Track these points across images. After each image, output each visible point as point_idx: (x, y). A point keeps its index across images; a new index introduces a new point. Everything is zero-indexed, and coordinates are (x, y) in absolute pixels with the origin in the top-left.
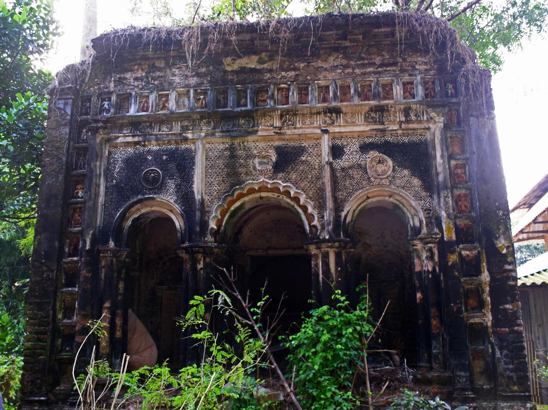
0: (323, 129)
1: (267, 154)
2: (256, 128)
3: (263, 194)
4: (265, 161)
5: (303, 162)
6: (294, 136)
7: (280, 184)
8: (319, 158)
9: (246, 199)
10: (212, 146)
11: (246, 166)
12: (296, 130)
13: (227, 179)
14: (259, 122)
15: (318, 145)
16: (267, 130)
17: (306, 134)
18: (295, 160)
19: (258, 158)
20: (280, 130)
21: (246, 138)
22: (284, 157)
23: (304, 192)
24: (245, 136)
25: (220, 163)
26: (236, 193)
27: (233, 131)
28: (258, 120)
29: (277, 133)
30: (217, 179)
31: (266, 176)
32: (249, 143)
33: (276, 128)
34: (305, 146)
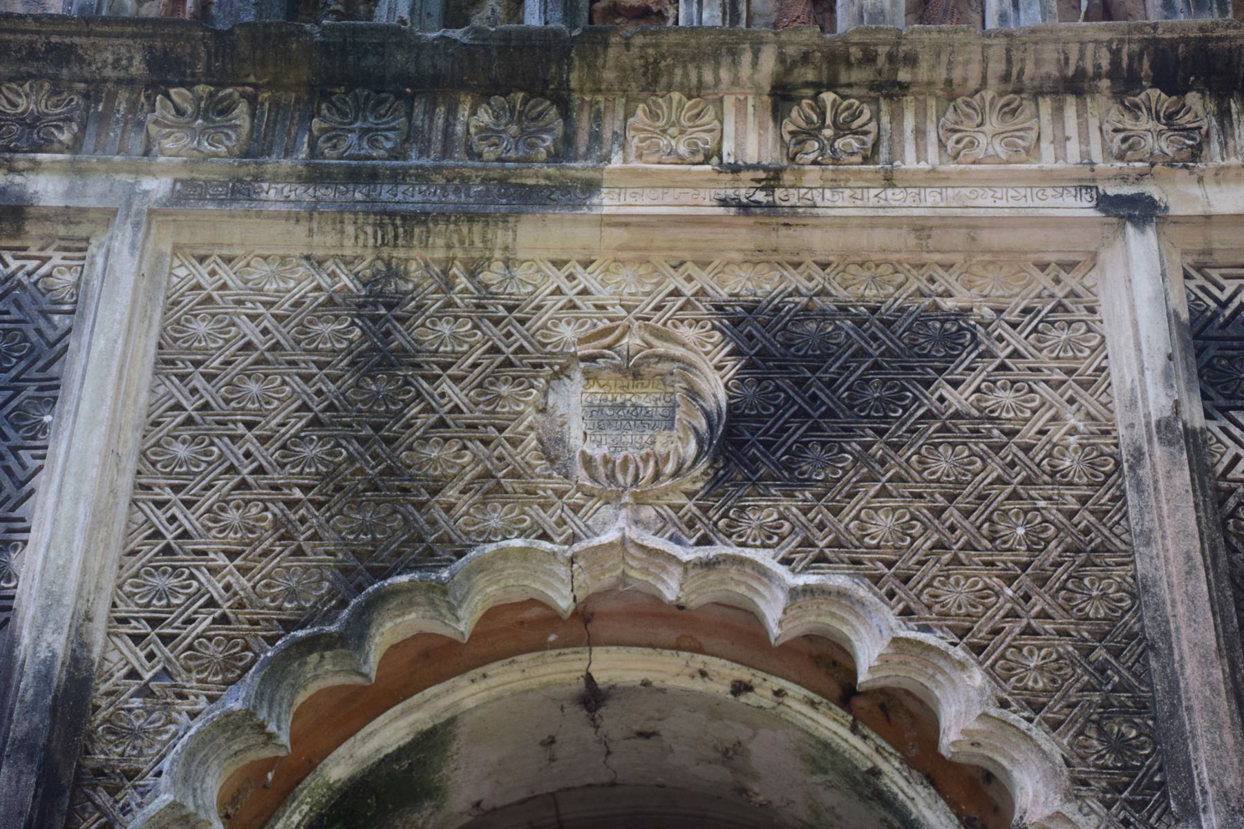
0: (1112, 191)
1: (661, 347)
2: (579, 168)
3: (615, 666)
4: (646, 398)
5: (949, 426)
6: (880, 238)
7: (762, 572)
8: (1088, 401)
9: (464, 694)
10: (225, 274)
11: (486, 430)
12: (894, 196)
13: (316, 518)
14: (610, 127)
15: (1066, 312)
16: (671, 183)
17: (972, 226)
18: (886, 404)
19: (588, 376)
20: (769, 188)
21: (500, 236)
22: (801, 383)
23: (977, 649)
24: (485, 218)
25: (280, 400)
26: (388, 631)
27: (397, 177)
28: (598, 117)
29: (745, 208)
30: (233, 516)
31: (648, 513)
32: (520, 272)
33: (735, 169)
34: (965, 312)
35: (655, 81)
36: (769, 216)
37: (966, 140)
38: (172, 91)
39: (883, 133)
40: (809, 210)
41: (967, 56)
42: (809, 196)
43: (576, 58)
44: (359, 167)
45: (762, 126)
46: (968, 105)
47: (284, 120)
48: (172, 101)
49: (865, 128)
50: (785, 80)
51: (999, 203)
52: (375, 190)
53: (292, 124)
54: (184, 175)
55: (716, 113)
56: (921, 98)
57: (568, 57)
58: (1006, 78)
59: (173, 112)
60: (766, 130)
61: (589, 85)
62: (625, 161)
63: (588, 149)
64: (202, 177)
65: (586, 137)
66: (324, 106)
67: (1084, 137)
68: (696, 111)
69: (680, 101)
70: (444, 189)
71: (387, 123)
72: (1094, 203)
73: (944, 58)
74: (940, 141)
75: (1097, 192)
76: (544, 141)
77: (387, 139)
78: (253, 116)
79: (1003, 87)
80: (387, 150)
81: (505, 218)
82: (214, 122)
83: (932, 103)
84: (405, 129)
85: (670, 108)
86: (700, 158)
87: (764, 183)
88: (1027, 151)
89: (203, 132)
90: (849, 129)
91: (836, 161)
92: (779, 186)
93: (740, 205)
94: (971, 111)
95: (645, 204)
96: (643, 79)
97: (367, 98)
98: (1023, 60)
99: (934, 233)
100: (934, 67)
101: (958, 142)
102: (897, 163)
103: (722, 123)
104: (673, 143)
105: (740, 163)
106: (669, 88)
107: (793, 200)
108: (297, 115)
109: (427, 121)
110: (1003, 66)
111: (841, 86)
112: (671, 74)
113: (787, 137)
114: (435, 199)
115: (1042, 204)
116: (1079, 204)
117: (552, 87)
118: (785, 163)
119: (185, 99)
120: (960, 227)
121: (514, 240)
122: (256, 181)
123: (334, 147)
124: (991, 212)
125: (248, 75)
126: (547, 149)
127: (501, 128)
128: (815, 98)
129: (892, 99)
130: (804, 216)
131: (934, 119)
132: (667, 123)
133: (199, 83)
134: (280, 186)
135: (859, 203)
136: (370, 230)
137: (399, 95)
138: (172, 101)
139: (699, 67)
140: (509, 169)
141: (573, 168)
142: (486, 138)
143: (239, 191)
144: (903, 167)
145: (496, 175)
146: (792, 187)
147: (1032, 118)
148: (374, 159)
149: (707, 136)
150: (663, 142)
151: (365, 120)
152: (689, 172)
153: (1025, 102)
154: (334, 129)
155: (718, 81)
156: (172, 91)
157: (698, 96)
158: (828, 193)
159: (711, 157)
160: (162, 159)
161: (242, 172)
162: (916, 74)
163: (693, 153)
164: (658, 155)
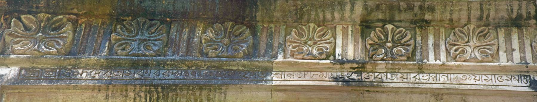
2: (261, 61)
16: (308, 69)
20: (359, 73)
27: (159, 66)
28: (271, 35)
29: (347, 82)
33: (342, 62)
35: (301, 18)
36: (359, 86)
37: (460, 50)
38: (23, 17)
39: (417, 45)
40: (379, 84)
41: (460, 7)
42: (379, 76)
43: (260, 5)
44: (138, 60)
45: (356, 41)
46: (461, 32)
47: (94, 34)
48: (22, 22)
49: (408, 43)
50: (368, 18)
51: (478, 83)
52: (146, 73)
53: (99, 36)
54: (27, 65)
55: (332, 34)
56: (437, 28)
57: (256, 5)
58: (480, 18)
59: (23, 28)
60: (358, 43)
61: (267, 19)
62: (285, 58)
63: (265, 51)
64: (40, 66)
65: (265, 45)
66: (118, 27)
67: (522, 50)
68: (322, 33)
69: (314, 27)
70: (186, 72)
71: (155, 36)
72: (528, 84)
73: (448, 8)
74: (447, 50)
75: (530, 78)
76: (242, 47)
77: (155, 45)
78: (75, 31)
79: (479, 23)
80: (154, 51)
81: (220, 87)
82: (49, 34)
83: (443, 30)
84: (166, 41)
85: (309, 31)
86: (324, 56)
87: (356, 70)
88: (492, 56)
89: (41, 41)
90: (400, 43)
91: (393, 59)
92: (364, 72)
93: (344, 81)
94: (463, 35)
95: (294, 80)
96: (295, 16)
97: (144, 23)
98: (489, 10)
99: (444, 97)
100: (443, 12)
101: (456, 50)
102: (425, 61)
103: (335, 39)
104: (310, 49)
105: (344, 59)
106: (309, 21)
107: (372, 79)
108: (102, 31)
109: (178, 36)
110: (479, 13)
111: (396, 21)
112: (309, 14)
113: (368, 47)
114: (181, 77)
115: (500, 84)
116: (520, 84)
117: (247, 19)
118: (368, 59)
119: (31, 21)
120: (458, 94)
121: (225, 98)
122: (75, 68)
123: (124, 49)
124: (474, 87)
125: (73, 9)
126: (244, 51)
127: (219, 40)
128: (383, 27)
129: (422, 28)
130: (377, 87)
131: (444, 38)
132: (307, 39)
133: (41, 12)
134: (89, 71)
135: (405, 81)
136: (143, 95)
137: (163, 22)
138: (22, 22)
139: (323, 11)
140: (223, 62)
141: (257, 61)
142: (211, 45)
143: (64, 75)
144: (428, 63)
145: (215, 65)
146: (371, 72)
147: (494, 39)
148: (147, 56)
149: (328, 46)
150: (305, 48)
151: (143, 34)
152: (318, 63)
153: (490, 31)
154: (124, 39)
155: (333, 18)
156: (23, 17)
157: (323, 25)
158: (389, 76)
159: (330, 56)
160: (13, 56)
161: (65, 63)
162: (434, 16)
163: (320, 54)
164: (302, 55)
